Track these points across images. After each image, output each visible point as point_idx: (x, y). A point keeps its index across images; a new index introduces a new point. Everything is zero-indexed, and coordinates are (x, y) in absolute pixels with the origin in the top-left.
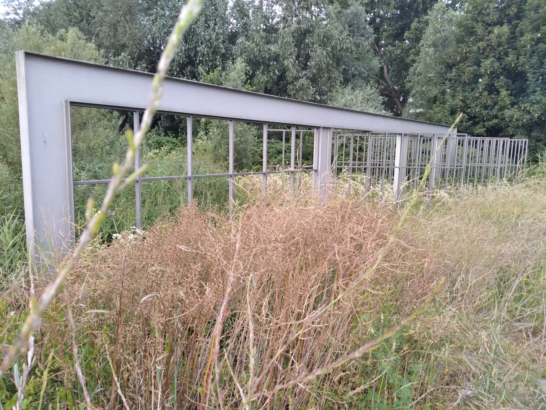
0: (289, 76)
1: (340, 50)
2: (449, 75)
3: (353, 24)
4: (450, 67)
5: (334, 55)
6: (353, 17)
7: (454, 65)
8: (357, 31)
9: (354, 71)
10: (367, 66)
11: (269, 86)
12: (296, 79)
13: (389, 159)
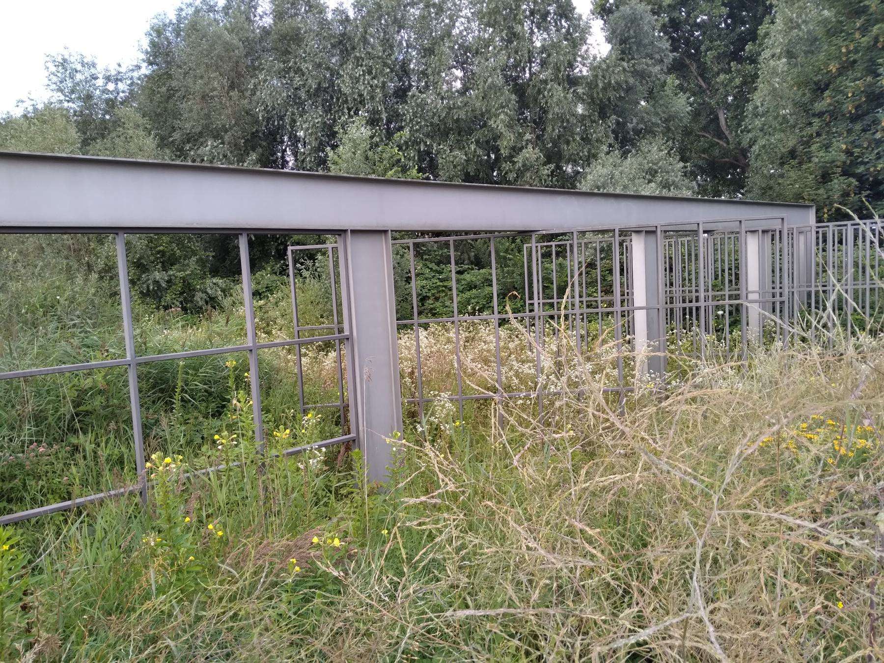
0: (505, 145)
1: (605, 89)
2: (819, 106)
3: (629, 38)
4: (820, 89)
5: (592, 98)
6: (626, 25)
7: (827, 86)
8: (637, 50)
9: (638, 124)
10: (664, 113)
11: (471, 169)
12: (516, 150)
13: (671, 284)
